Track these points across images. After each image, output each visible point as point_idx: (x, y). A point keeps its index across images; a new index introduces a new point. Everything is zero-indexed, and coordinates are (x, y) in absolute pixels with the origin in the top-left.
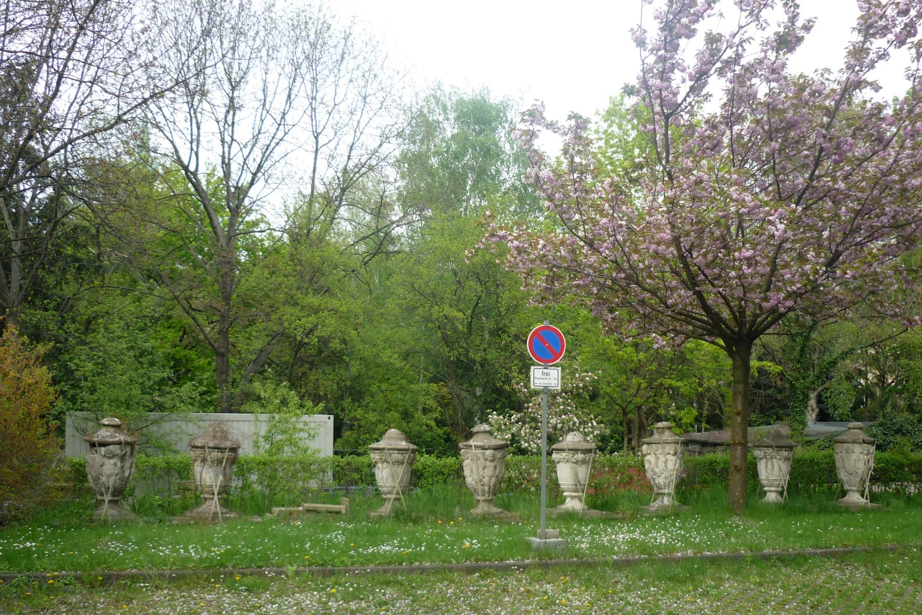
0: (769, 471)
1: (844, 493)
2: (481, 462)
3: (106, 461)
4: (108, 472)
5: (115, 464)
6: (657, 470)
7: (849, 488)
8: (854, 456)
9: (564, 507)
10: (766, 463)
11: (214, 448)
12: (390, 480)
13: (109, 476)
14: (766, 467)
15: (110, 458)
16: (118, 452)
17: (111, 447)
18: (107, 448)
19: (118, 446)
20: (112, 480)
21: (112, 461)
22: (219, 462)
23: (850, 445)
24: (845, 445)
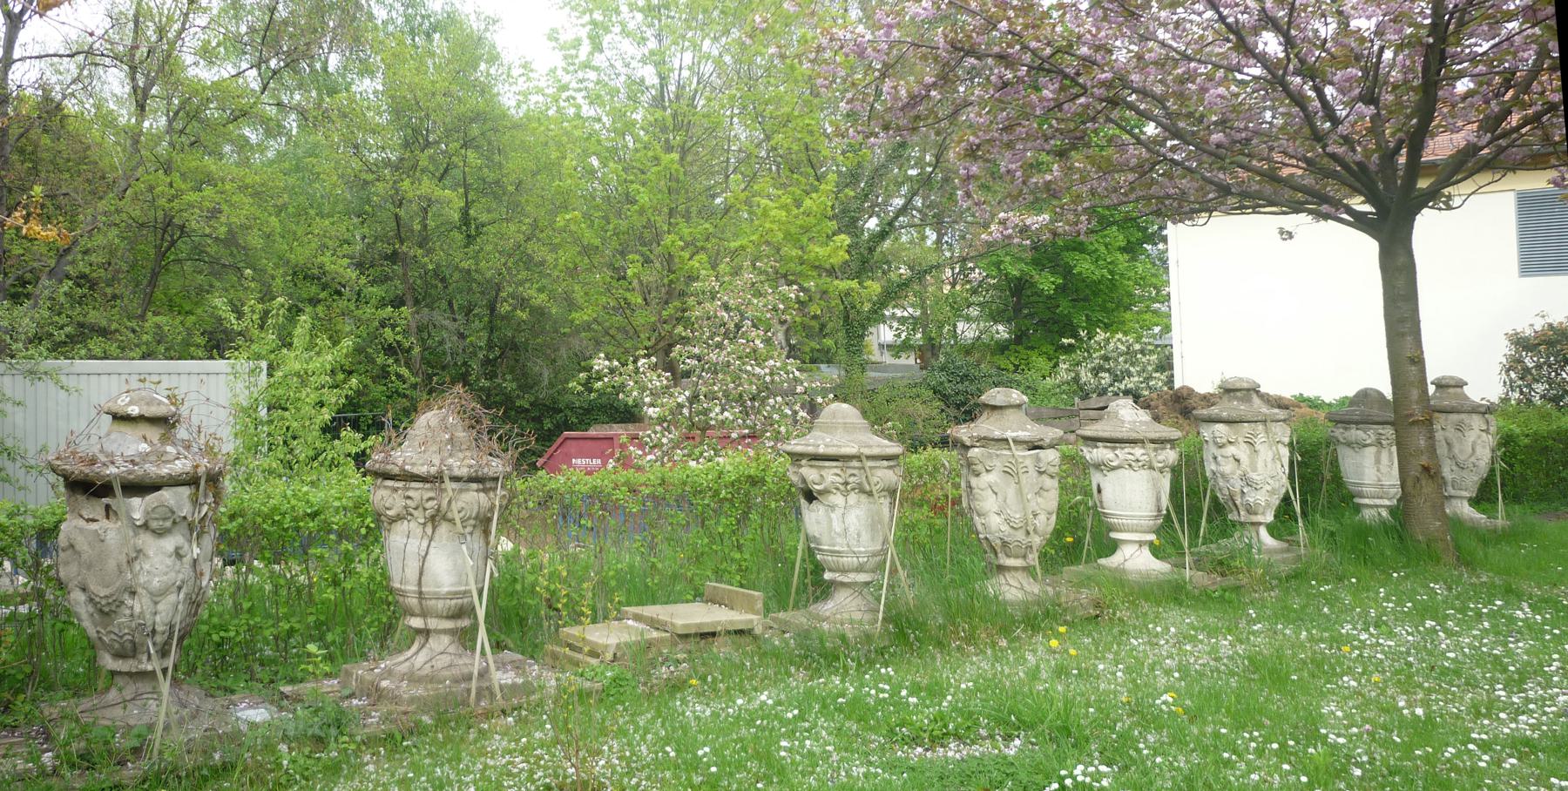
0: (1384, 469)
1: (1112, 547)
2: (1030, 479)
3: (145, 540)
4: (156, 583)
5: (178, 554)
6: (1254, 476)
7: (1452, 492)
8: (1471, 436)
9: (1114, 561)
10: (1378, 454)
11: (471, 480)
12: (865, 537)
13: (157, 597)
14: (1378, 461)
15: (160, 533)
16: (186, 510)
17: (166, 495)
18: (152, 499)
19: (185, 491)
20: (165, 606)
21: (169, 543)
22: (483, 522)
23: (1463, 416)
24: (1454, 417)
